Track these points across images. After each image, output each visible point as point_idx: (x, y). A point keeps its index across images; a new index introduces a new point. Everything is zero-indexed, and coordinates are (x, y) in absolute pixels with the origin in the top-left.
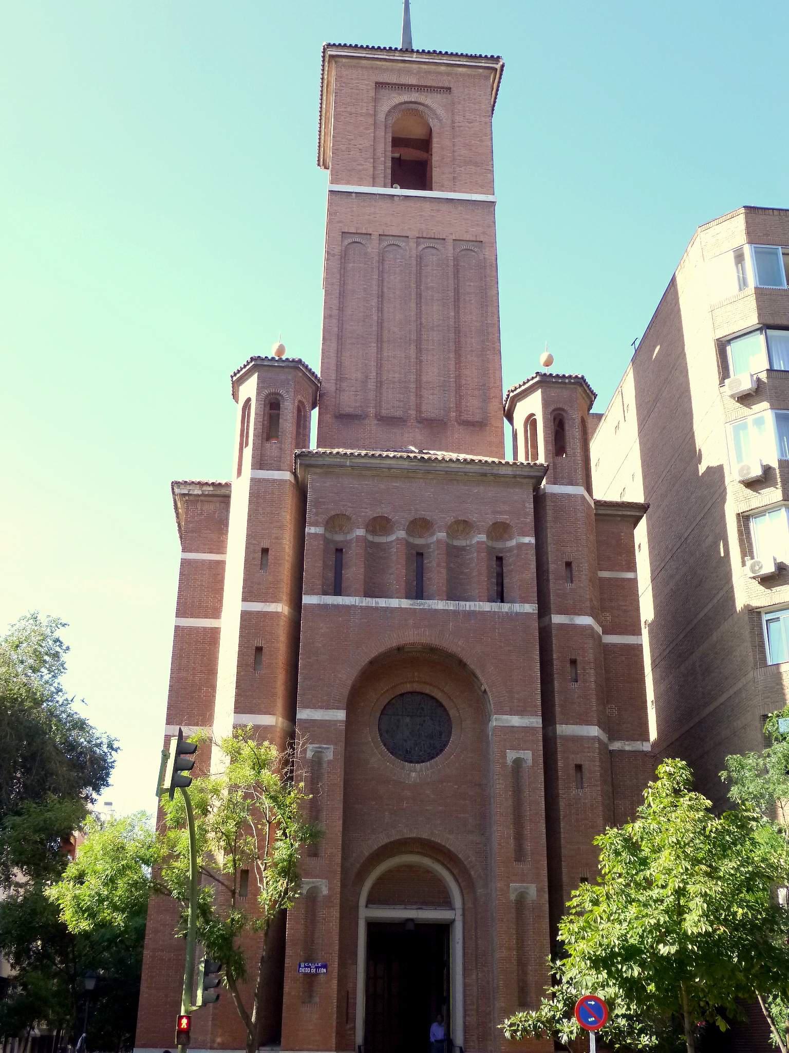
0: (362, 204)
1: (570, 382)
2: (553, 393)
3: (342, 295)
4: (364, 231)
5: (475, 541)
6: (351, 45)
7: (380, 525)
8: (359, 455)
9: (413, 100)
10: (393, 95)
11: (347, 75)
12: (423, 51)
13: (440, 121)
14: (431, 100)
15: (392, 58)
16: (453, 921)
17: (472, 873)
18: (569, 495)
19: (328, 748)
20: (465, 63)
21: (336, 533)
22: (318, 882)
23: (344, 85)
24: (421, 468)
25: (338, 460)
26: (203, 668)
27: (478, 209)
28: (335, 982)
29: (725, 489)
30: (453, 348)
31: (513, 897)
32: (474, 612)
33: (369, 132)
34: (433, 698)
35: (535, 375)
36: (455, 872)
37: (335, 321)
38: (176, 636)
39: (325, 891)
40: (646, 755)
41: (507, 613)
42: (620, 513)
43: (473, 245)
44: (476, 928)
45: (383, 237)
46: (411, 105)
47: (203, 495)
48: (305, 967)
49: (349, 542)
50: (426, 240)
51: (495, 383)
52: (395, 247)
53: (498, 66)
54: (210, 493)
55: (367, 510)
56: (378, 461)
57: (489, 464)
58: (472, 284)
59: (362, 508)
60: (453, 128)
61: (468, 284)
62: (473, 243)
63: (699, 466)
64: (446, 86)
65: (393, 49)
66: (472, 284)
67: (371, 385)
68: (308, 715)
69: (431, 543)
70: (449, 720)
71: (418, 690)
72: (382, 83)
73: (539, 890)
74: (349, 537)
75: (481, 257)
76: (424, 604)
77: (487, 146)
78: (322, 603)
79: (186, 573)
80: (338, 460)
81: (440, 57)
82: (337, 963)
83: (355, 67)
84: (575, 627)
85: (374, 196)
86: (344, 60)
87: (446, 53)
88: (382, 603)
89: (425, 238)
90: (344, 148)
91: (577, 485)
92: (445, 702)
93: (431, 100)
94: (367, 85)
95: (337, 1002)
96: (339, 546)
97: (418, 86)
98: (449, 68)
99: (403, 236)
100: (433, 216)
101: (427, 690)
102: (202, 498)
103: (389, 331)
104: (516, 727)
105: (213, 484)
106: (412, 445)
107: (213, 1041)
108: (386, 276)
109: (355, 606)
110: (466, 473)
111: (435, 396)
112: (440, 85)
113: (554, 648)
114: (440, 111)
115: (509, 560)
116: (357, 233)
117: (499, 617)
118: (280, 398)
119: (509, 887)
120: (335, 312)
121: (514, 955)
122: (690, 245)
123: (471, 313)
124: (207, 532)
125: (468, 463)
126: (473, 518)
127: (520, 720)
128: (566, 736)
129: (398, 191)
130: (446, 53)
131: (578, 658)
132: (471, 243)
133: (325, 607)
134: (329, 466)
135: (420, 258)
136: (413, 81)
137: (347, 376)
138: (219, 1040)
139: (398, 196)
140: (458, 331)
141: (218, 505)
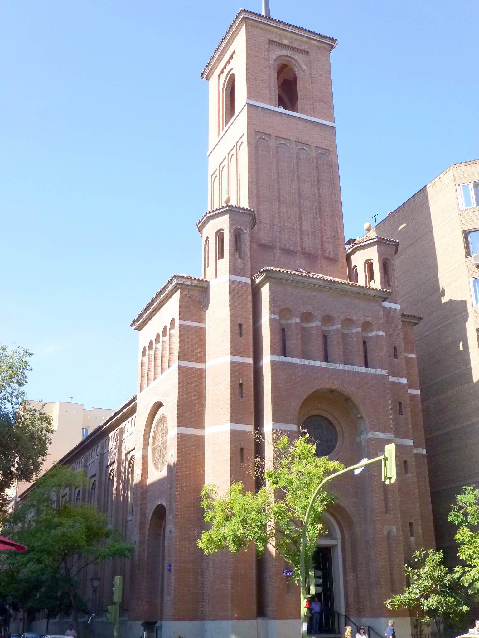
2: (384, 249)
3: (257, 170)
4: (267, 132)
5: (293, 321)
6: (314, 32)
7: (307, 317)
8: (345, 283)
12: (296, 26)
13: (303, 71)
14: (299, 57)
15: (278, 26)
16: (336, 545)
17: (354, 519)
18: (394, 309)
23: (251, 37)
24: (329, 286)
25: (286, 276)
26: (196, 393)
29: (467, 314)
30: (318, 212)
32: (358, 372)
33: (266, 70)
34: (326, 419)
35: (375, 237)
37: (255, 186)
38: (179, 372)
40: (424, 456)
42: (409, 320)
43: (325, 151)
45: (278, 138)
47: (192, 286)
48: (286, 572)
49: (290, 325)
50: (300, 144)
51: (341, 236)
52: (283, 145)
53: (334, 45)
54: (196, 285)
55: (301, 308)
56: (307, 279)
57: (277, 272)
58: (325, 175)
59: (298, 306)
60: (311, 77)
61: (323, 174)
63: (442, 298)
65: (335, 39)
66: (325, 175)
67: (277, 229)
68: (278, 427)
70: (336, 432)
71: (320, 414)
72: (272, 41)
73: (398, 529)
74: (289, 322)
75: (330, 160)
76: (332, 366)
78: (280, 361)
79: (182, 333)
81: (305, 32)
83: (256, 27)
85: (271, 112)
86: (250, 21)
89: (300, 143)
91: (397, 303)
92: (335, 422)
93: (299, 57)
94: (263, 40)
96: (284, 327)
97: (291, 47)
98: (308, 40)
99: (288, 139)
100: (303, 130)
101: (325, 414)
102: (190, 287)
104: (381, 439)
106: (300, 268)
107: (233, 615)
108: (279, 162)
109: (297, 364)
110: (350, 292)
111: (310, 240)
112: (303, 49)
114: (303, 65)
115: (370, 344)
116: (263, 133)
118: (241, 232)
119: (383, 527)
120: (254, 180)
122: (443, 174)
124: (192, 308)
126: (354, 318)
129: (281, 110)
131: (402, 402)
134: (281, 279)
135: (298, 154)
136: (288, 43)
137: (262, 221)
138: (236, 615)
139: (284, 114)
140: (320, 203)
141: (198, 292)
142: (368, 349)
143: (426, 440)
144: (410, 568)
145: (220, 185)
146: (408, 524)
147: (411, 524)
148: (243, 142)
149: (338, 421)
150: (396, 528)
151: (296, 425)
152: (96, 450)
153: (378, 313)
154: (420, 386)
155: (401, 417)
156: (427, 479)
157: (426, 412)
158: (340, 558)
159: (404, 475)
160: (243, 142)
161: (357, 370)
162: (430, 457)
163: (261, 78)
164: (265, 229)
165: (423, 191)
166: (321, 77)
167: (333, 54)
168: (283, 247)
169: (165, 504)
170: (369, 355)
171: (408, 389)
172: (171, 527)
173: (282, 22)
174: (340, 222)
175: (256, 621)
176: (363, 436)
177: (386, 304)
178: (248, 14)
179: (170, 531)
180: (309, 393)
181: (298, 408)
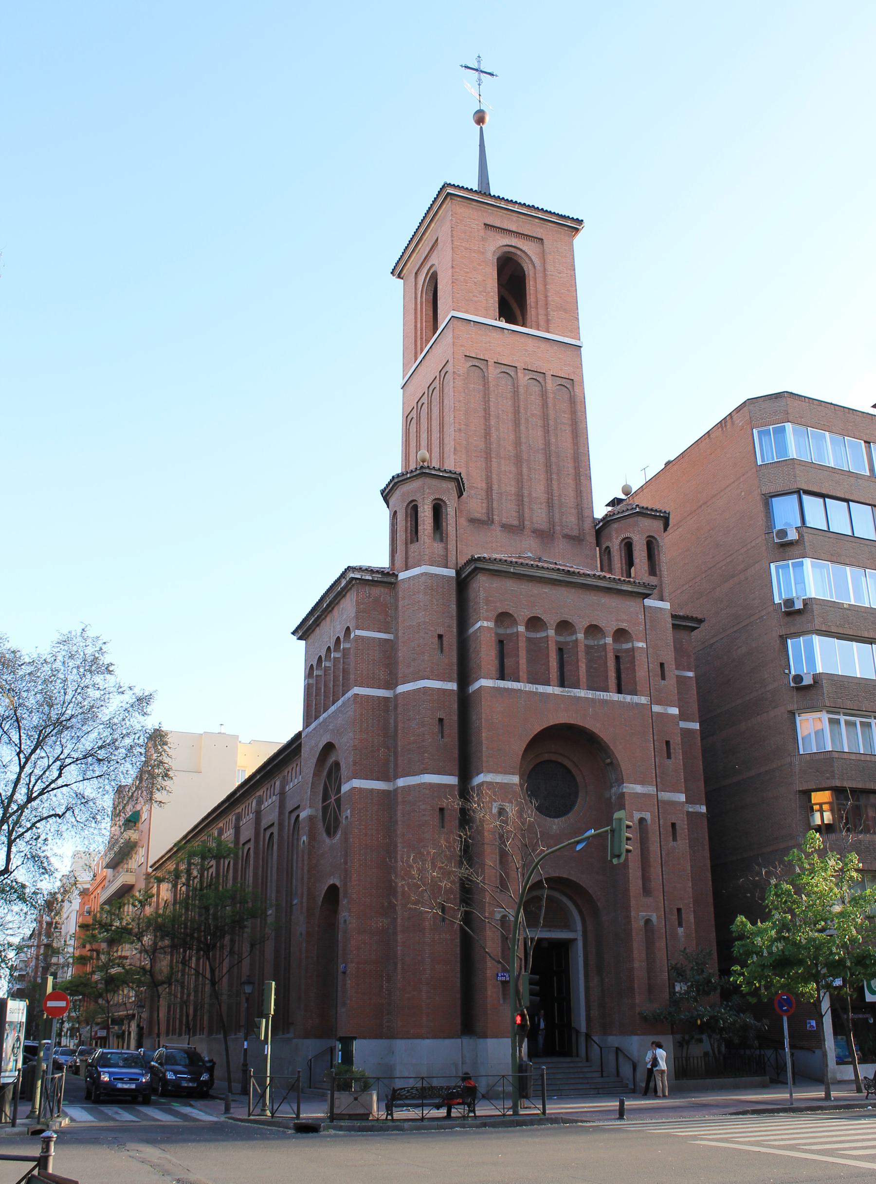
0: (479, 332)
9: (513, 245)
10: (497, 237)
11: (461, 213)
14: (529, 248)
15: (498, 205)
16: (576, 939)
17: (599, 904)
20: (555, 220)
27: (568, 351)
32: (606, 701)
41: (629, 702)
46: (511, 248)
48: (502, 976)
50: (530, 372)
51: (588, 505)
54: (379, 579)
58: (566, 416)
62: (566, 380)
64: (539, 237)
69: (570, 642)
73: (658, 917)
77: (573, 297)
84: (667, 714)
87: (542, 209)
88: (541, 689)
90: (462, 280)
92: (574, 770)
94: (477, 225)
99: (512, 366)
101: (560, 759)
103: (505, 449)
112: (534, 235)
114: (535, 259)
119: (639, 915)
123: (566, 442)
124: (375, 613)
125: (601, 579)
126: (601, 624)
127: (641, 788)
128: (664, 800)
129: (503, 324)
130: (542, 209)
132: (564, 380)
133: (498, 689)
142: (622, 667)
143: (706, 793)
144: (773, 914)
145: (418, 432)
146: (676, 911)
147: (679, 910)
148: (447, 372)
150: (657, 915)
152: (273, 787)
153: (638, 616)
154: (699, 717)
155: (669, 762)
156: (707, 847)
157: (708, 753)
159: (672, 844)
160: (447, 372)
161: (605, 698)
162: (713, 817)
163: (473, 279)
164: (479, 497)
165: (709, 436)
166: (560, 275)
167: (579, 241)
168: (505, 522)
169: (338, 883)
170: (623, 676)
171: (680, 722)
172: (345, 916)
174: (586, 484)
175: (459, 1040)
176: (614, 790)
177: (648, 602)
178: (451, 188)
179: (345, 921)
180: (538, 729)
181: (521, 753)
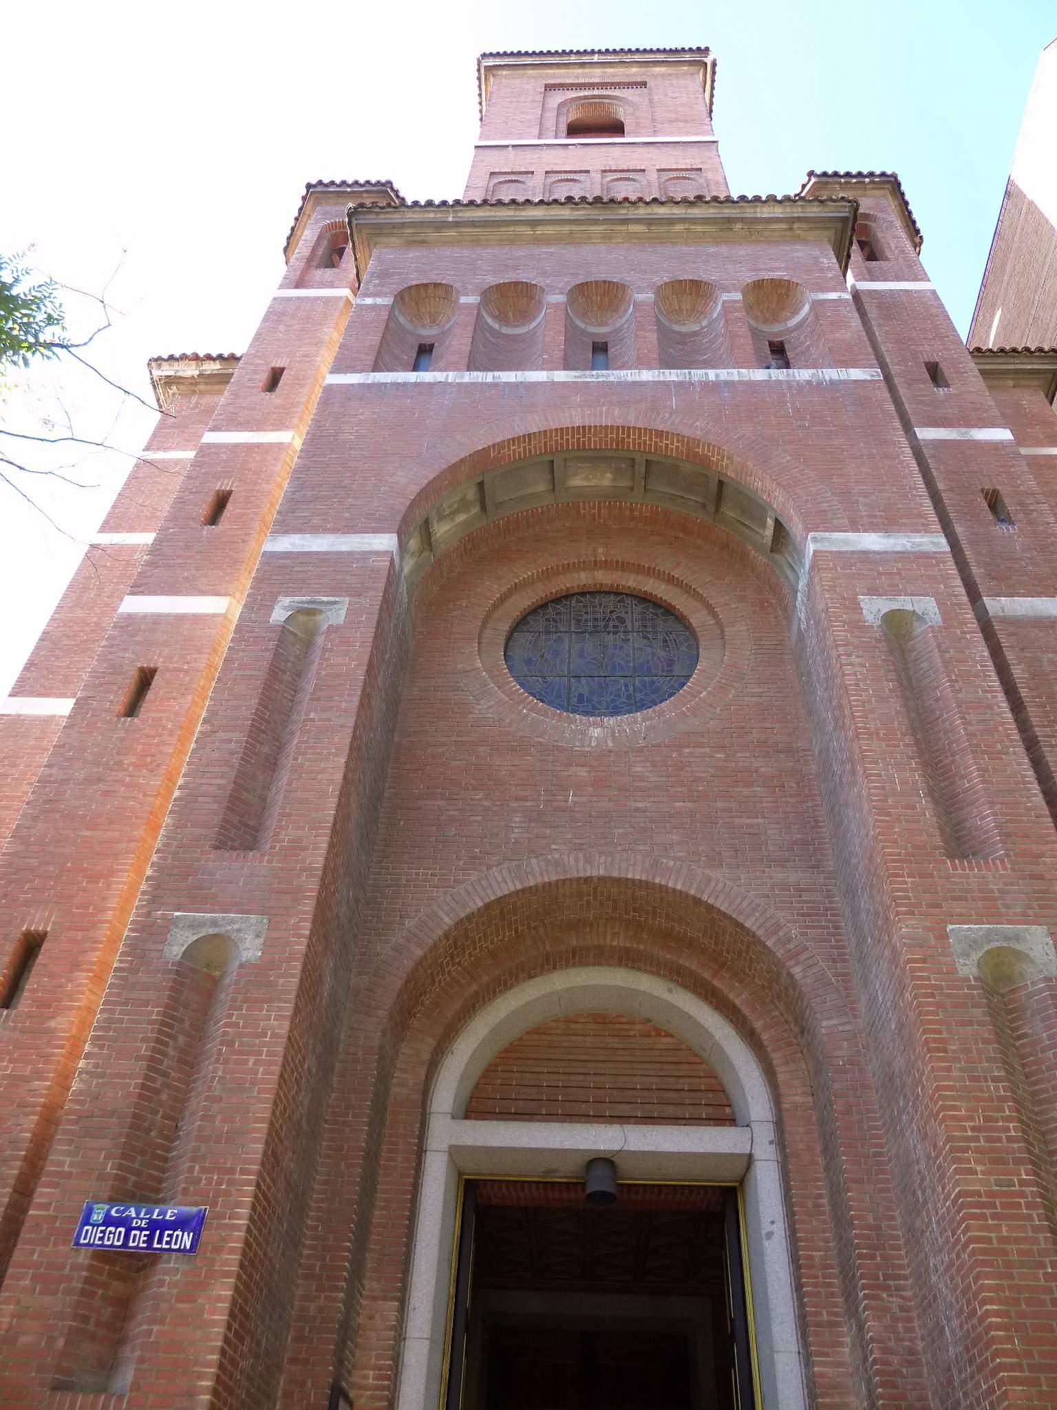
1: (872, 182)
17: (797, 971)
19: (335, 603)
21: (423, 326)
22: (232, 921)
25: (432, 215)
28: (224, 1290)
31: (967, 968)
34: (645, 599)
36: (739, 999)
39: (250, 949)
44: (829, 1151)
48: (108, 1221)
56: (511, 213)
80: (432, 215)
82: (245, 1211)
95: (215, 1393)
101: (631, 581)
105: (220, 357)
113: (935, 474)
117: (790, 387)
119: (943, 936)
121: (1023, 1183)
149: (696, 595)
151: (394, 537)
158: (770, 1235)
173: (571, 51)
